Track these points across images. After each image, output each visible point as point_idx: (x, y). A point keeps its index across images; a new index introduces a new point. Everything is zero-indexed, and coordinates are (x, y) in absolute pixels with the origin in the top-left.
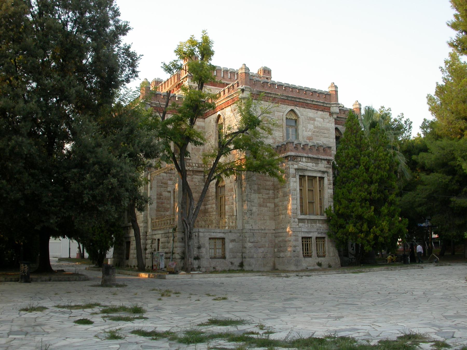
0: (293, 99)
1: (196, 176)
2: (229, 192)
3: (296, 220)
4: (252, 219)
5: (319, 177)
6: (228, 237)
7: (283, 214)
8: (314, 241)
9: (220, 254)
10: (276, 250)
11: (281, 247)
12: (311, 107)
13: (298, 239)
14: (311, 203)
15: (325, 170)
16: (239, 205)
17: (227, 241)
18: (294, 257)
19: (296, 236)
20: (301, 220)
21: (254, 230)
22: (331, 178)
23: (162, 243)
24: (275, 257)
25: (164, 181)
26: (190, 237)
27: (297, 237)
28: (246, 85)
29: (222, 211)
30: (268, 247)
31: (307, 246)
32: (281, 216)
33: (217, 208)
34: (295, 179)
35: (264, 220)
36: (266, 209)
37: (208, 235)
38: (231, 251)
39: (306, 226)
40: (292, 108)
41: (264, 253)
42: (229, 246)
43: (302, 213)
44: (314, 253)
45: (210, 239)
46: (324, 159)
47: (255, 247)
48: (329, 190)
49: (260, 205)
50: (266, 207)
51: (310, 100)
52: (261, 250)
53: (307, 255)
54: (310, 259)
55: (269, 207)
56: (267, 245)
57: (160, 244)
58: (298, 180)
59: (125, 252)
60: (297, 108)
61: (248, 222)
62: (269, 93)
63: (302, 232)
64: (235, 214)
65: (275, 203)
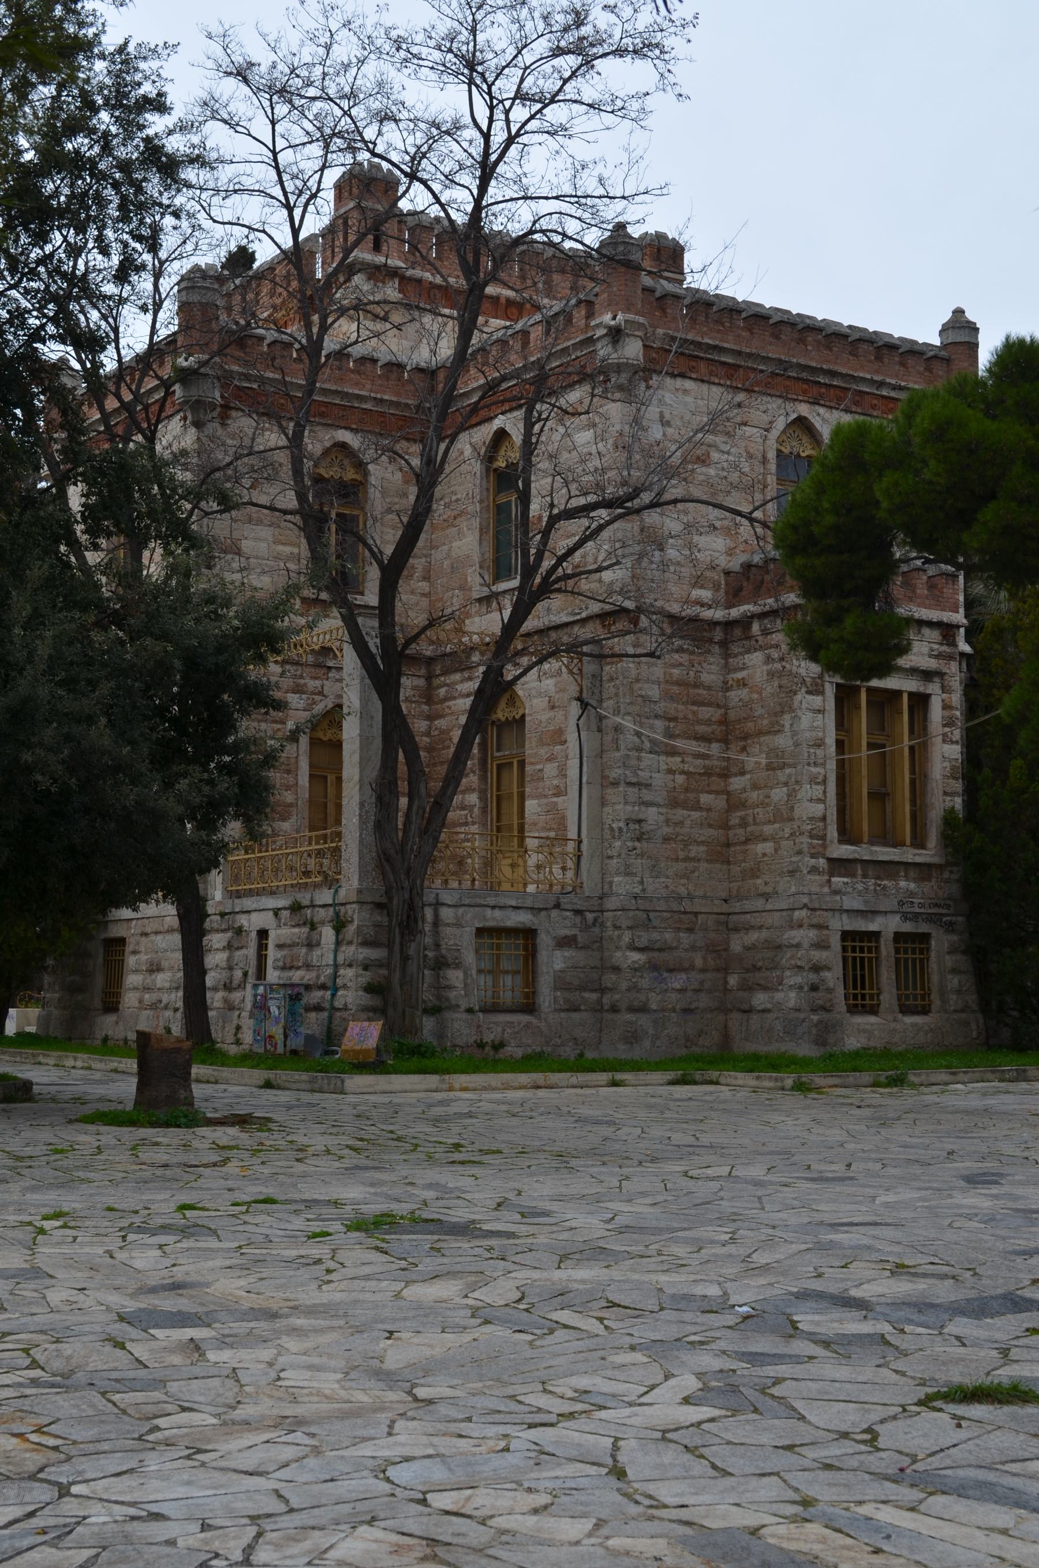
0: (804, 375)
2: (542, 743)
3: (822, 862)
4: (642, 855)
5: (911, 694)
6: (552, 927)
7: (765, 840)
8: (886, 948)
10: (733, 981)
11: (756, 969)
12: (874, 407)
14: (880, 797)
15: (932, 664)
16: (590, 797)
17: (544, 940)
18: (813, 1010)
19: (820, 927)
20: (839, 866)
21: (650, 899)
22: (956, 698)
23: (280, 946)
24: (727, 1011)
27: (825, 932)
28: (627, 309)
29: (505, 821)
31: (862, 968)
32: (761, 848)
33: (484, 810)
34: (820, 698)
35: (687, 859)
36: (696, 815)
37: (473, 920)
38: (561, 983)
39: (860, 887)
40: (804, 410)
42: (553, 961)
43: (846, 835)
44: (888, 997)
45: (480, 932)
46: (930, 624)
47: (654, 967)
48: (947, 747)
49: (674, 803)
50: (697, 807)
51: (872, 382)
52: (677, 981)
53: (861, 1001)
54: (872, 1019)
56: (699, 963)
57: (272, 953)
58: (831, 705)
59: (99, 981)
60: (822, 410)
61: (627, 866)
62: (715, 348)
63: (842, 911)
64: (572, 834)
65: (728, 793)
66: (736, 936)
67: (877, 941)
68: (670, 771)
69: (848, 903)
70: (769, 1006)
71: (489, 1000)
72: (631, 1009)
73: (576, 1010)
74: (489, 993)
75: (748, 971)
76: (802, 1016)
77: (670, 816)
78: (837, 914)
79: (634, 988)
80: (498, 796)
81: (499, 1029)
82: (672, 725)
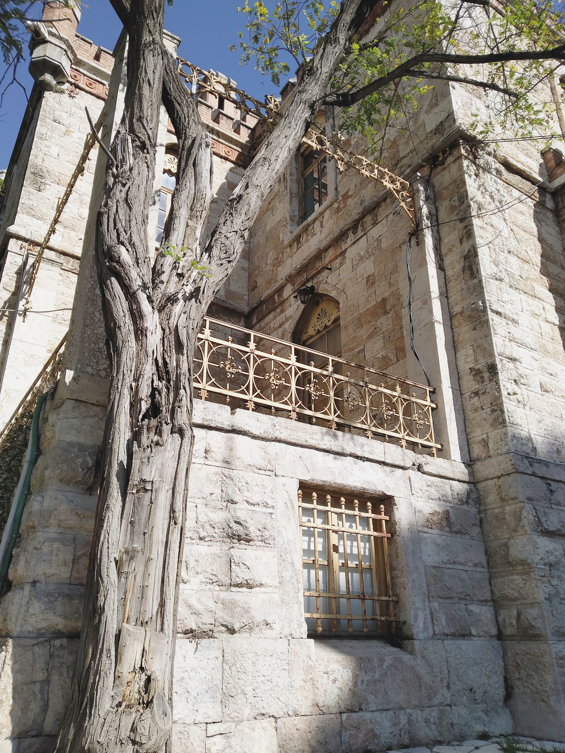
26: (155, 410)
45: (307, 490)
73: (465, 635)
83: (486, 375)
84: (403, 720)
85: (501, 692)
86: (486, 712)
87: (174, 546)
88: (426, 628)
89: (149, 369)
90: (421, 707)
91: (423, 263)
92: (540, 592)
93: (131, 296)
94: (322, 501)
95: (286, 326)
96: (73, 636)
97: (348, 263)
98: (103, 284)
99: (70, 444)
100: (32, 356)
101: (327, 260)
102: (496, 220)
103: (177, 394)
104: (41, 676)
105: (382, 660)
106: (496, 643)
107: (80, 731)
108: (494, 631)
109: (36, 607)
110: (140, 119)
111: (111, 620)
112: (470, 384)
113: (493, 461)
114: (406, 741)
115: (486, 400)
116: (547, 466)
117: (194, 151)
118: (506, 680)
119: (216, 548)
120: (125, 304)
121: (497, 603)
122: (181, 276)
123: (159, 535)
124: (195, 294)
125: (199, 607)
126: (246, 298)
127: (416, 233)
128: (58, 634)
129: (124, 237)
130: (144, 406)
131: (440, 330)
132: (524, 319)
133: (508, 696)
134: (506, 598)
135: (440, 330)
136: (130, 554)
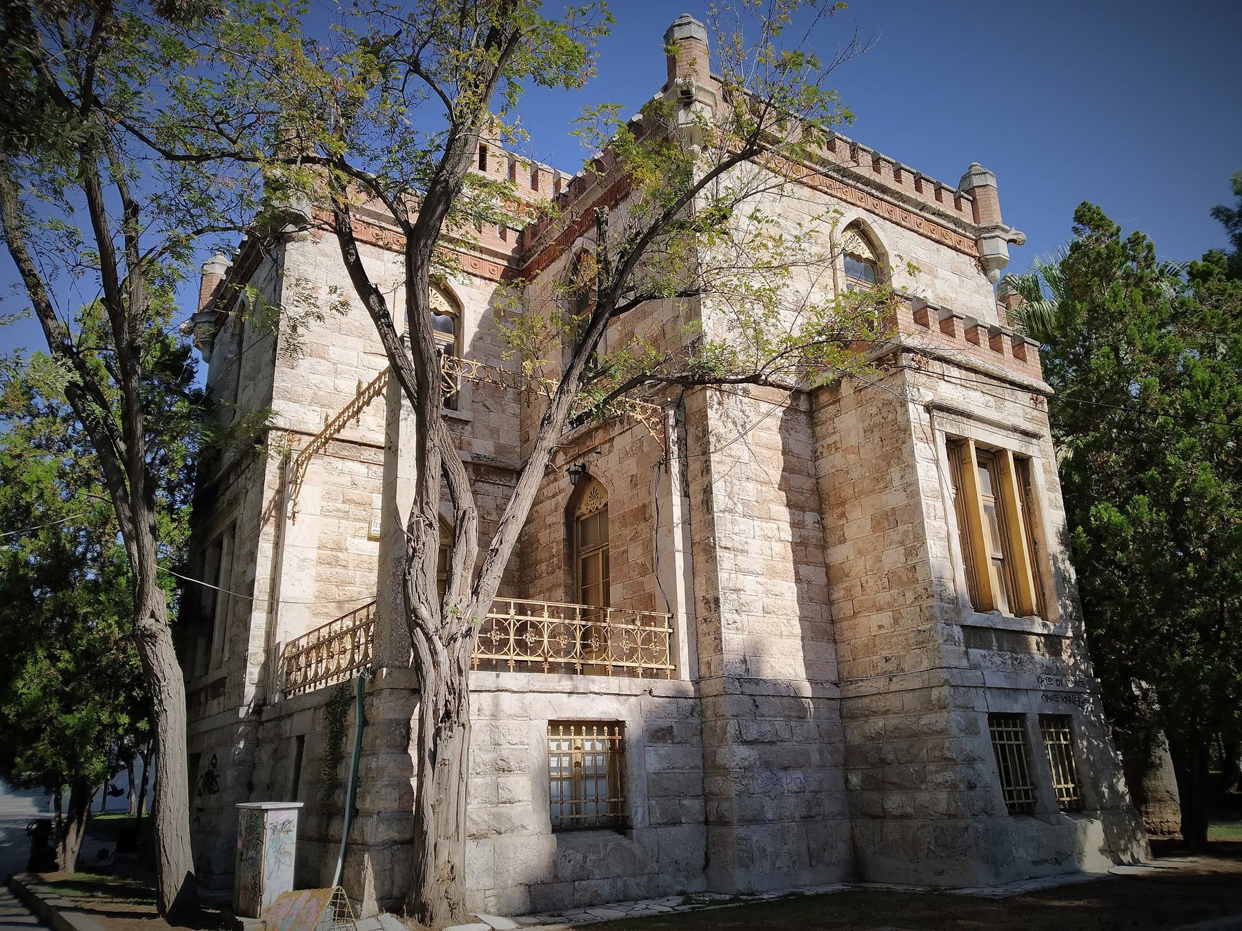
1: (486, 486)
3: (957, 632)
7: (879, 610)
9: (604, 807)
13: (976, 720)
25: (354, 494)
26: (448, 714)
30: (822, 767)
38: (658, 788)
39: (997, 660)
41: (808, 795)
45: (554, 725)
47: (766, 765)
52: (792, 781)
55: (809, 583)
56: (815, 757)
66: (854, 724)
67: (1023, 725)
68: (767, 538)
69: (994, 680)
70: (910, 810)
71: (567, 816)
72: (745, 821)
73: (676, 823)
74: (566, 806)
75: (874, 766)
76: (962, 824)
77: (769, 587)
78: (980, 691)
79: (746, 793)
80: (584, 590)
81: (580, 856)
82: (764, 488)
83: (713, 606)
84: (620, 884)
85: (702, 862)
86: (687, 877)
87: (463, 794)
88: (643, 820)
89: (443, 689)
90: (635, 876)
91: (669, 493)
92: (733, 789)
93: (429, 639)
94: (567, 731)
95: (560, 497)
96: (410, 842)
97: (615, 453)
98: (411, 631)
99: (391, 721)
100: (304, 560)
101: (597, 442)
102: (738, 449)
103: (460, 702)
104: (389, 866)
105: (606, 846)
106: (703, 827)
107: (419, 894)
108: (702, 819)
109: (382, 828)
110: (427, 503)
111: (431, 838)
112: (702, 611)
113: (712, 681)
114: (621, 897)
115: (711, 627)
116: (757, 684)
117: (465, 523)
118: (706, 854)
119: (488, 779)
120: (426, 645)
121: (707, 796)
122: (459, 619)
123: (454, 789)
124: (468, 633)
125: (479, 820)
126: (518, 449)
127: (665, 462)
128: (395, 842)
129: (423, 598)
130: (441, 713)
131: (679, 559)
132: (755, 546)
133: (706, 866)
134: (712, 793)
135: (679, 559)
136: (439, 802)
